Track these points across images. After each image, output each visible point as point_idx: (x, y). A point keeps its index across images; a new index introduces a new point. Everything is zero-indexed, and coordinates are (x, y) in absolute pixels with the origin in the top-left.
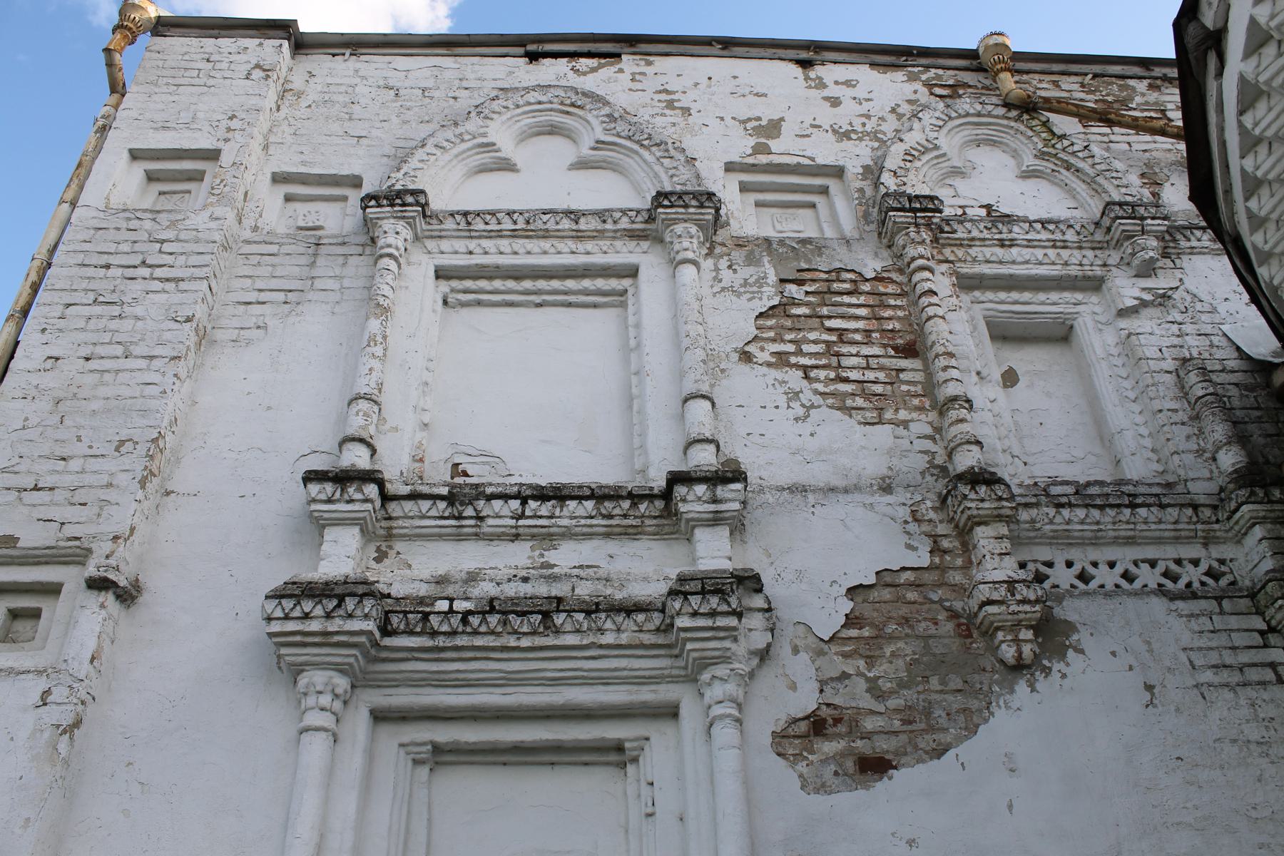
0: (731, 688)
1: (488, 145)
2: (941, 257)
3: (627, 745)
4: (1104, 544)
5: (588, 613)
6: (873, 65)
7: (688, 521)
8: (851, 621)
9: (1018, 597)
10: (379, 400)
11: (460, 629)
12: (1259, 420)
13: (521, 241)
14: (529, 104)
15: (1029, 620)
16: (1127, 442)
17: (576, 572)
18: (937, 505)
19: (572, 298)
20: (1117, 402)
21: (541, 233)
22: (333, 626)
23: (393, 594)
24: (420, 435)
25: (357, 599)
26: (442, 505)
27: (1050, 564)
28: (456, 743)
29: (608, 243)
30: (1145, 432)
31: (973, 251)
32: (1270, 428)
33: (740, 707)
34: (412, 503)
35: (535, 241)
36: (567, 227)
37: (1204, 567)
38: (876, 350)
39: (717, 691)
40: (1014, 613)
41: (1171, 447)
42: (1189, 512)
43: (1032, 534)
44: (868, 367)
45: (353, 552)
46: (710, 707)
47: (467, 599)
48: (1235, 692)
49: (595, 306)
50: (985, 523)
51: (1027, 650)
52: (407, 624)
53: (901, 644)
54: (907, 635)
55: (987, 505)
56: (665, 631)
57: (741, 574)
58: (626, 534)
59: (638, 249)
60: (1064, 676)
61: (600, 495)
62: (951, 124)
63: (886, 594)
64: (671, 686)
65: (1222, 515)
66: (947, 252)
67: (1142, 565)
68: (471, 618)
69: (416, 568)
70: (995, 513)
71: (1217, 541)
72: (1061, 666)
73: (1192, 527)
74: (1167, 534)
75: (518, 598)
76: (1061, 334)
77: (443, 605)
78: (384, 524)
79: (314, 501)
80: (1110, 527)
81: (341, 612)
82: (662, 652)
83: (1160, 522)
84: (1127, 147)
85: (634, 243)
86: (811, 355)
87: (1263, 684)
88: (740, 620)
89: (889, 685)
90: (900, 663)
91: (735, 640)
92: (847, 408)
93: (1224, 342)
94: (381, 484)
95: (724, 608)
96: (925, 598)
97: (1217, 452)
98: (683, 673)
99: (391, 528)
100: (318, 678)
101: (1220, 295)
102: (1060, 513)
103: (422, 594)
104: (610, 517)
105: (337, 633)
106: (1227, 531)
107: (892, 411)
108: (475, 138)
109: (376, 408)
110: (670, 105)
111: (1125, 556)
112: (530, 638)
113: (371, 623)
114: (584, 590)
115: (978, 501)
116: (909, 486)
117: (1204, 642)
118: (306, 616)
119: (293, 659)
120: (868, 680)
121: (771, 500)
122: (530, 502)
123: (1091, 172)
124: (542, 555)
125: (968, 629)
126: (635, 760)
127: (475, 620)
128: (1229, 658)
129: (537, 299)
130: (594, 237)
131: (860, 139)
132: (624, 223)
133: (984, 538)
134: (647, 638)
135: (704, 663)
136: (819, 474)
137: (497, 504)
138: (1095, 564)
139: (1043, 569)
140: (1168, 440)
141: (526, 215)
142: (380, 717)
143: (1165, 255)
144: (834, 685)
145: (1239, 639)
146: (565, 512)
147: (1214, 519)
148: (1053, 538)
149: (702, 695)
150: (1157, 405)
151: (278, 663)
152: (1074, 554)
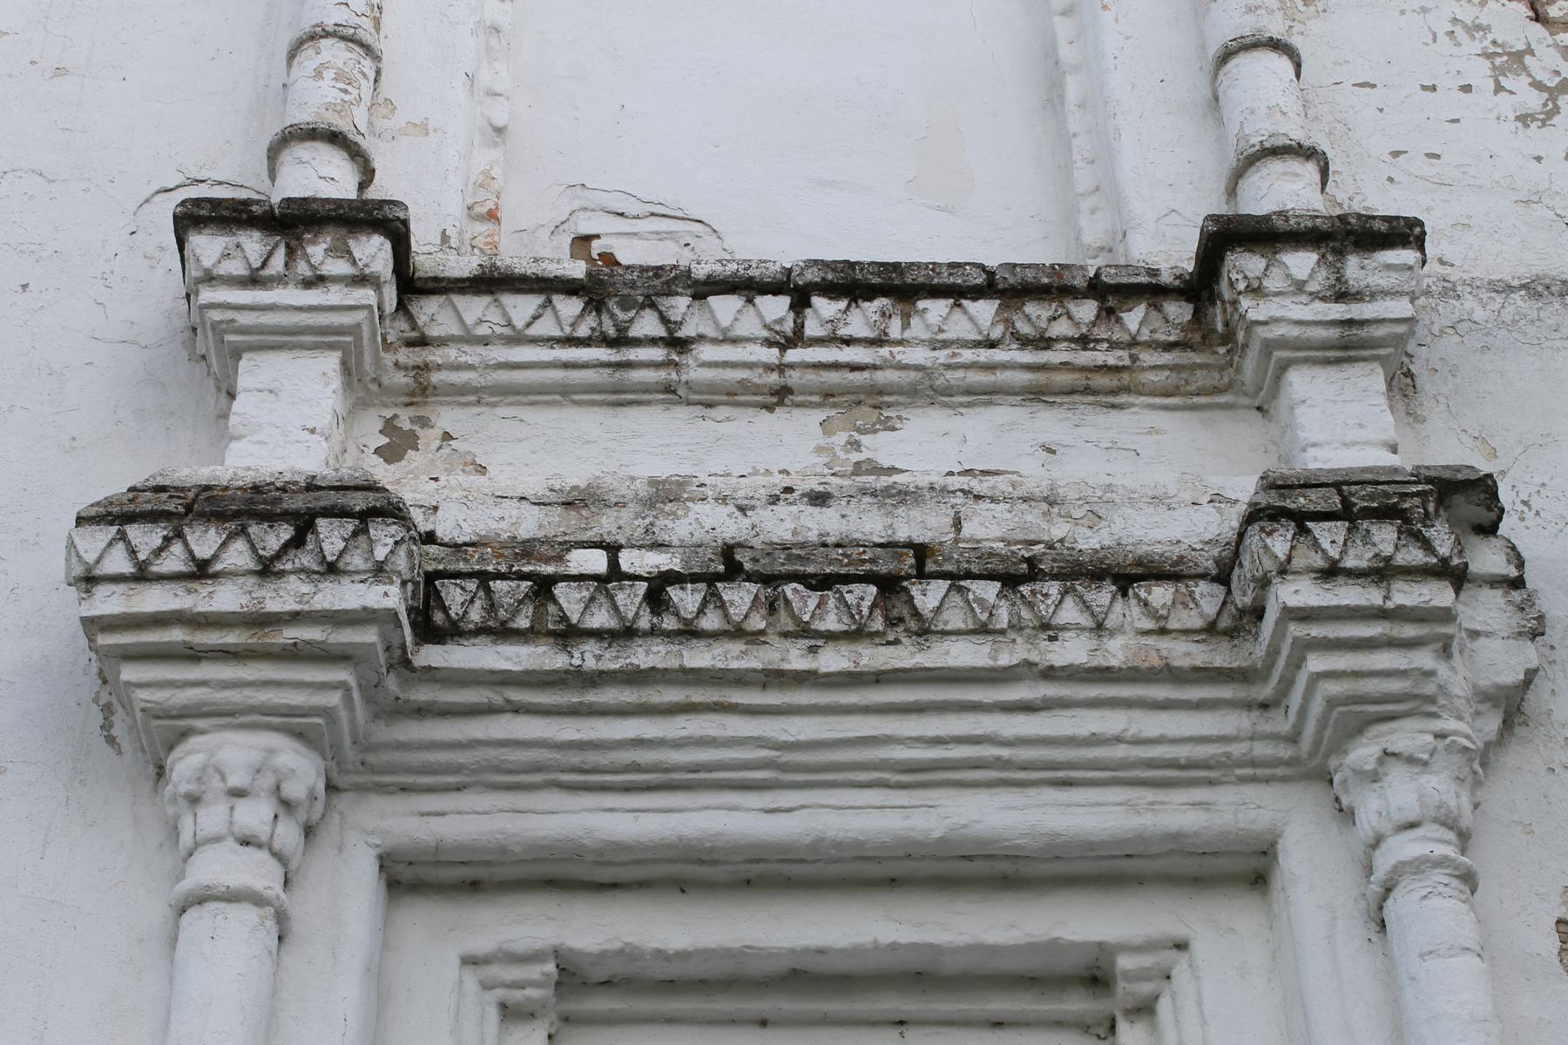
0: (1439, 786)
3: (1125, 962)
5: (1010, 581)
7: (1269, 346)
10: (376, 45)
11: (644, 623)
17: (957, 482)
22: (282, 597)
23: (444, 531)
24: (484, 158)
25: (350, 525)
26: (570, 307)
28: (630, 954)
33: (1464, 837)
34: (485, 300)
39: (1403, 793)
45: (324, 420)
46: (1377, 842)
47: (658, 546)
52: (492, 607)
56: (1231, 634)
57: (1447, 475)
58: (1087, 390)
61: (1009, 289)
64: (1250, 791)
68: (674, 593)
69: (494, 474)
75: (802, 545)
77: (596, 562)
78: (406, 356)
79: (210, 278)
81: (305, 559)
82: (1225, 692)
88: (1458, 591)
91: (1446, 651)
94: (399, 236)
95: (1413, 555)
98: (1285, 752)
99: (425, 368)
100: (237, 751)
103: (526, 531)
104: (1043, 342)
105: (295, 618)
109: (368, 65)
112: (845, 648)
113: (394, 590)
114: (988, 527)
118: (201, 571)
119: (159, 695)
121: (1479, 314)
122: (818, 301)
124: (855, 445)
126: (1144, 1010)
127: (687, 599)
134: (1184, 653)
135: (1357, 716)
137: (725, 307)
142: (407, 878)
146: (917, 329)
149: (1346, 814)
151: (107, 726)
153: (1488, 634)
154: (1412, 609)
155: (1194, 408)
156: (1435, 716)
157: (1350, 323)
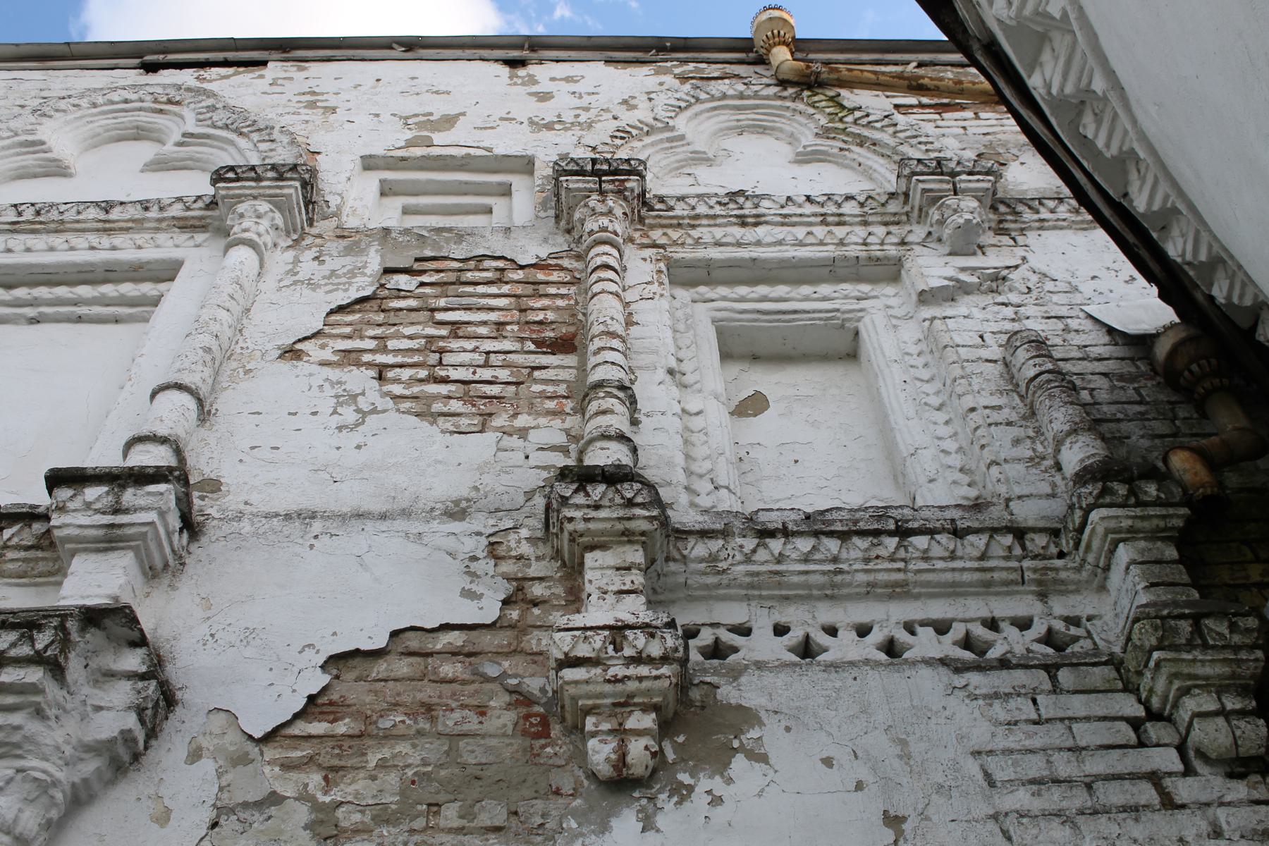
1: (33, 143)
2: (645, 241)
4: (849, 597)
6: (608, 62)
8: (313, 706)
9: (628, 652)
12: (1141, 417)
13: (22, 237)
14: (112, 103)
15: (648, 692)
16: (927, 462)
18: (539, 534)
19: (82, 310)
20: (912, 413)
21: (53, 226)
27: (744, 631)
29: (147, 236)
30: (951, 445)
31: (695, 233)
32: (1160, 427)
35: (44, 236)
36: (91, 217)
37: (1039, 629)
38: (507, 345)
40: (616, 680)
41: (988, 455)
42: (1008, 540)
43: (711, 580)
44: (487, 365)
48: (1075, 826)
49: (117, 320)
50: (602, 547)
51: (638, 750)
53: (403, 747)
54: (420, 733)
55: (603, 514)
59: (191, 243)
60: (716, 801)
62: (698, 108)
63: (403, 667)
65: (1066, 543)
66: (656, 235)
67: (919, 630)
70: (620, 526)
71: (1063, 588)
72: (717, 784)
73: (1014, 564)
74: (966, 577)
76: (844, 348)
80: (858, 566)
83: (953, 556)
84: (962, 131)
85: (186, 236)
86: (397, 351)
87: (1134, 810)
89: (357, 817)
90: (392, 779)
92: (432, 415)
93: (1088, 325)
96: (476, 673)
97: (1057, 451)
101: (1085, 271)
102: (766, 546)
106: (1078, 570)
107: (505, 416)
108: (16, 135)
110: (312, 105)
111: (889, 617)
115: (592, 511)
116: (498, 510)
117: (1016, 739)
120: (317, 807)
122: (154, 683)
123: (892, 142)
125: (545, 723)
128: (1064, 766)
129: (30, 312)
130: (128, 229)
131: (566, 129)
132: (177, 210)
133: (599, 569)
136: (350, 496)
138: (832, 631)
139: (728, 637)
140: (983, 447)
141: (37, 207)
143: (1001, 231)
144: (242, 815)
145: (1086, 734)
147: (1053, 550)
148: (751, 586)
150: (969, 401)
152: (789, 614)
153: (109, 709)
154: (11, 684)
155: (36, 585)
156: (20, 757)
157: (112, 526)
